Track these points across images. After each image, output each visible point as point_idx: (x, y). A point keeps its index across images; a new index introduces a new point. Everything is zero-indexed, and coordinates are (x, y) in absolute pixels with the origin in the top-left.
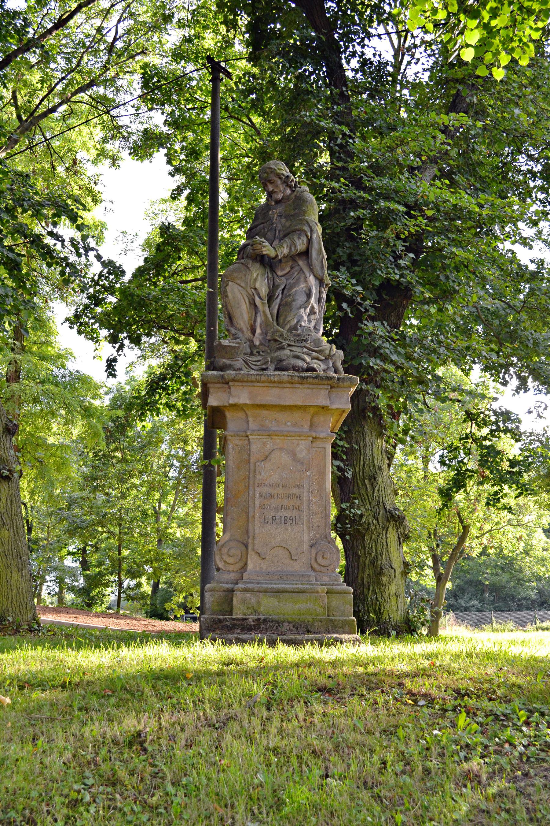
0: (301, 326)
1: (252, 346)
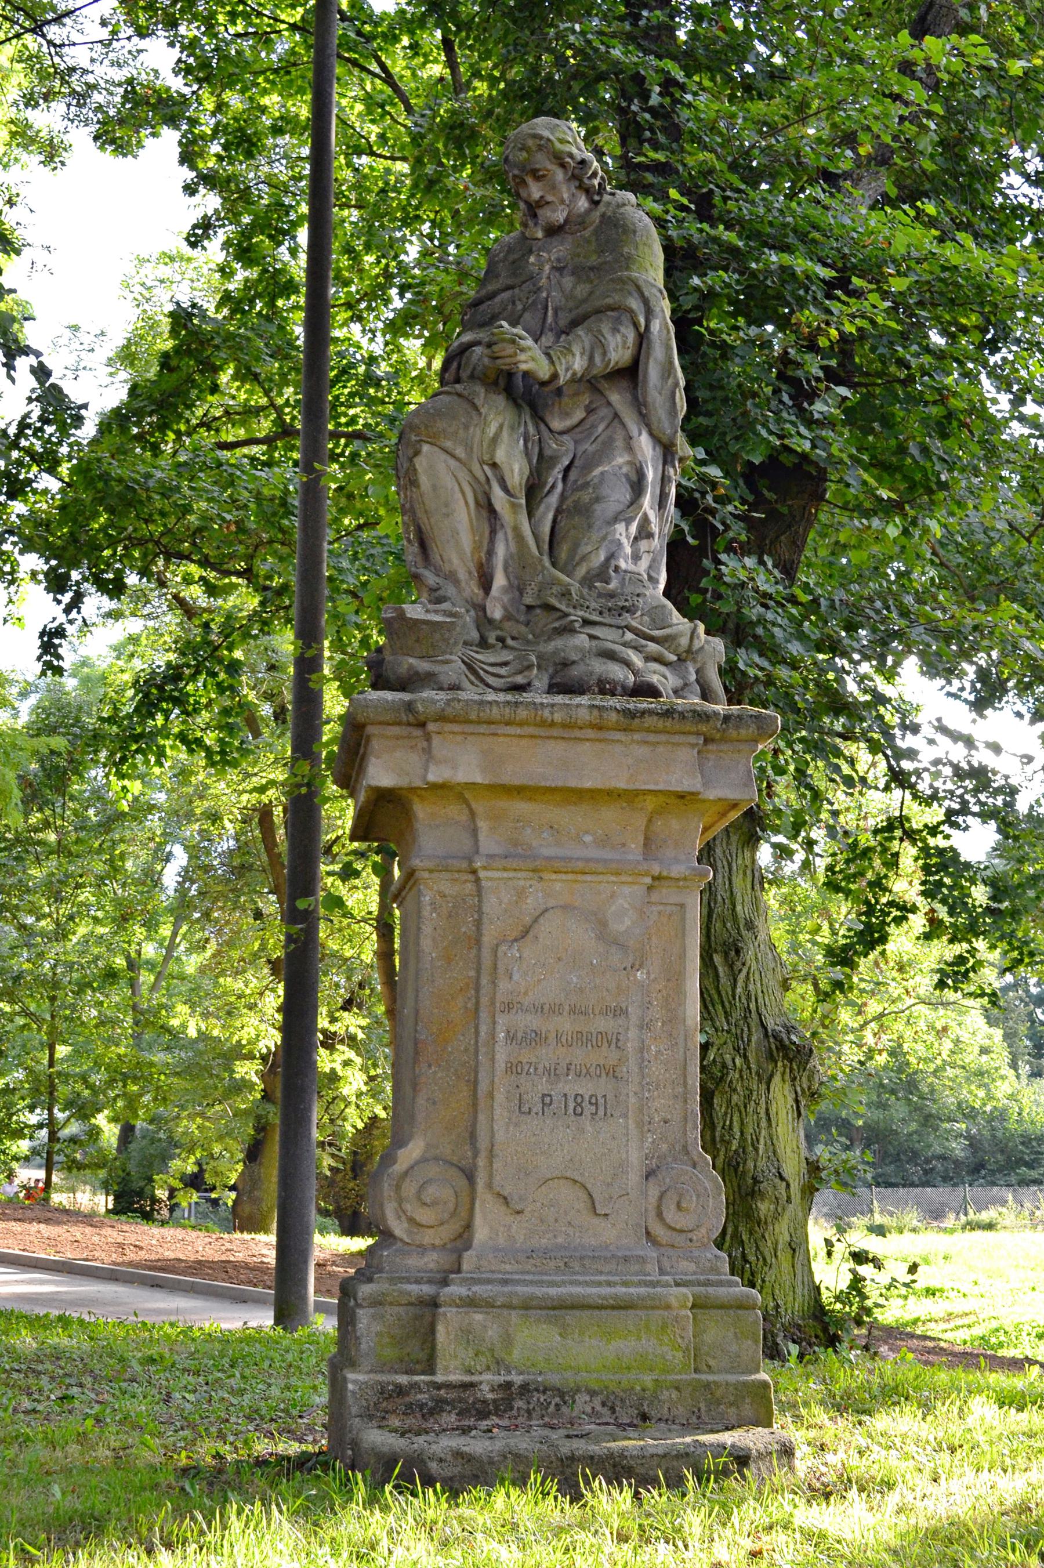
0: (617, 569)
1: (484, 621)
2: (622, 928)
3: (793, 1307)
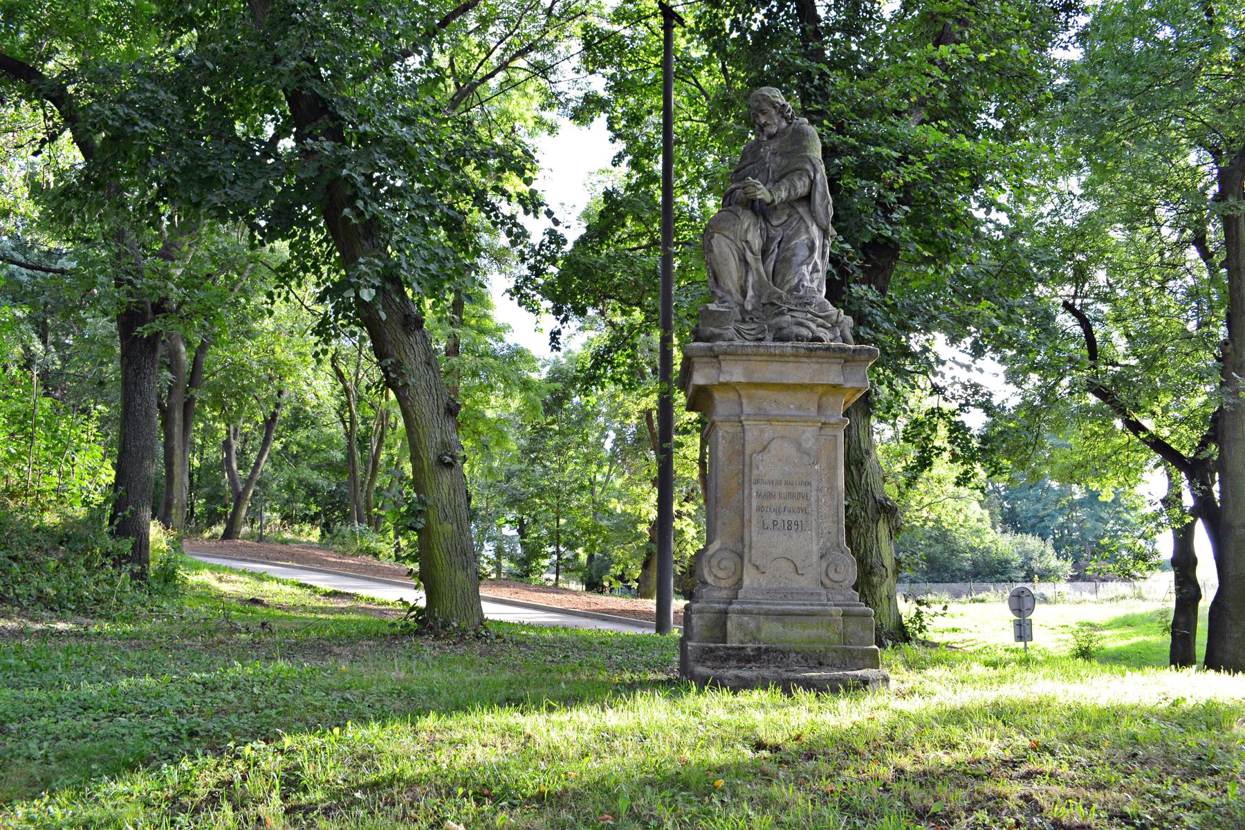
3: (889, 624)
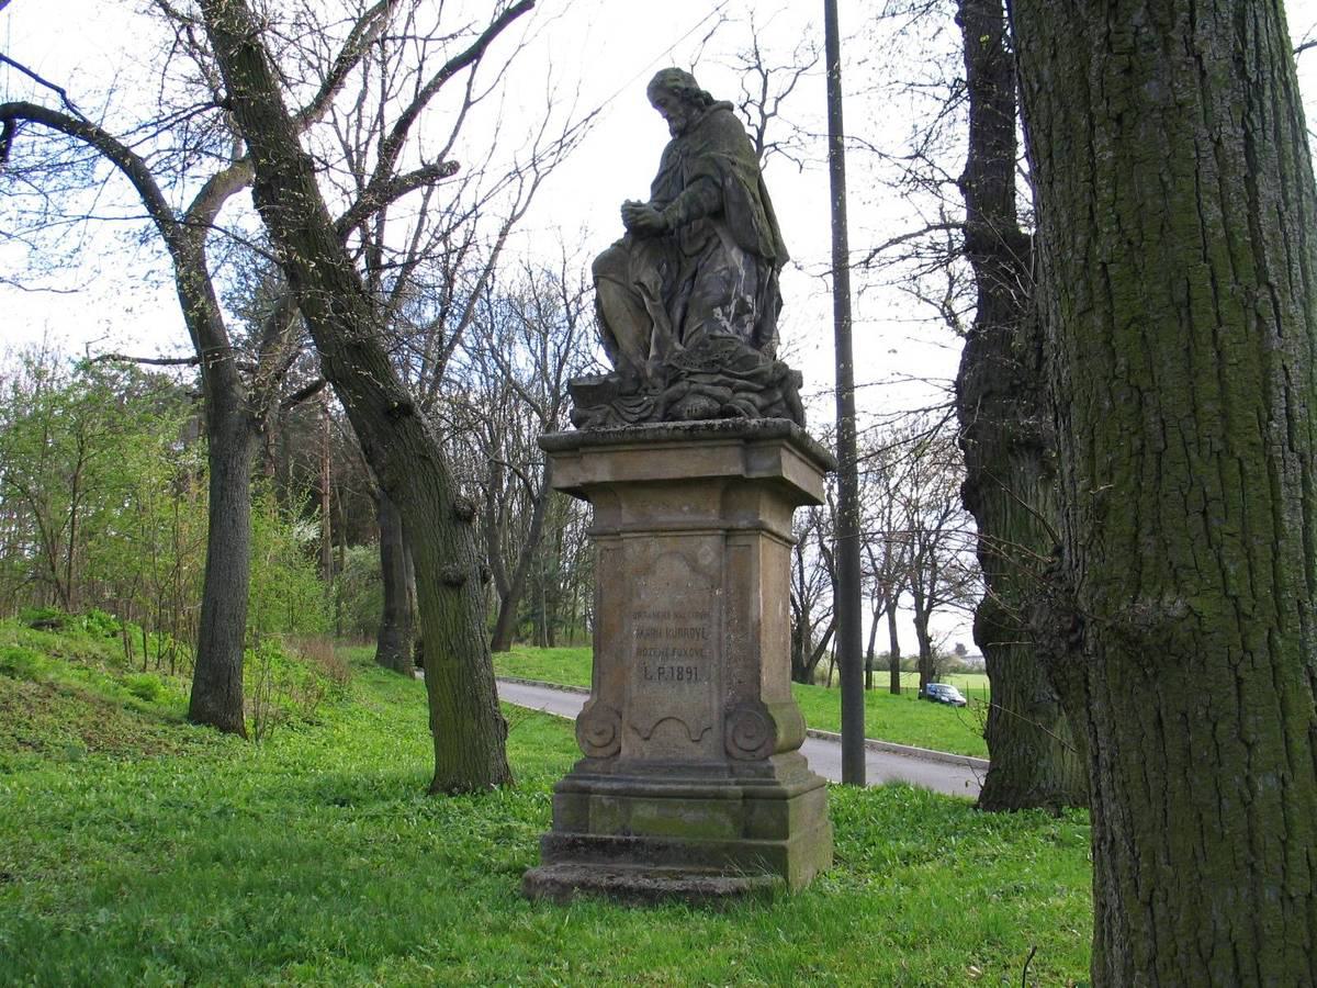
2: (707, 563)
